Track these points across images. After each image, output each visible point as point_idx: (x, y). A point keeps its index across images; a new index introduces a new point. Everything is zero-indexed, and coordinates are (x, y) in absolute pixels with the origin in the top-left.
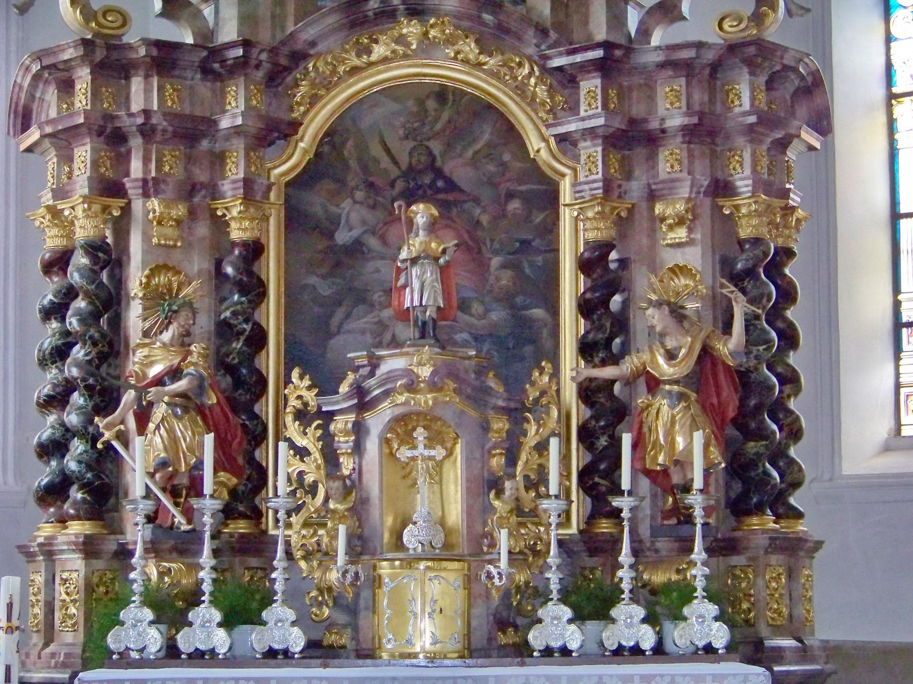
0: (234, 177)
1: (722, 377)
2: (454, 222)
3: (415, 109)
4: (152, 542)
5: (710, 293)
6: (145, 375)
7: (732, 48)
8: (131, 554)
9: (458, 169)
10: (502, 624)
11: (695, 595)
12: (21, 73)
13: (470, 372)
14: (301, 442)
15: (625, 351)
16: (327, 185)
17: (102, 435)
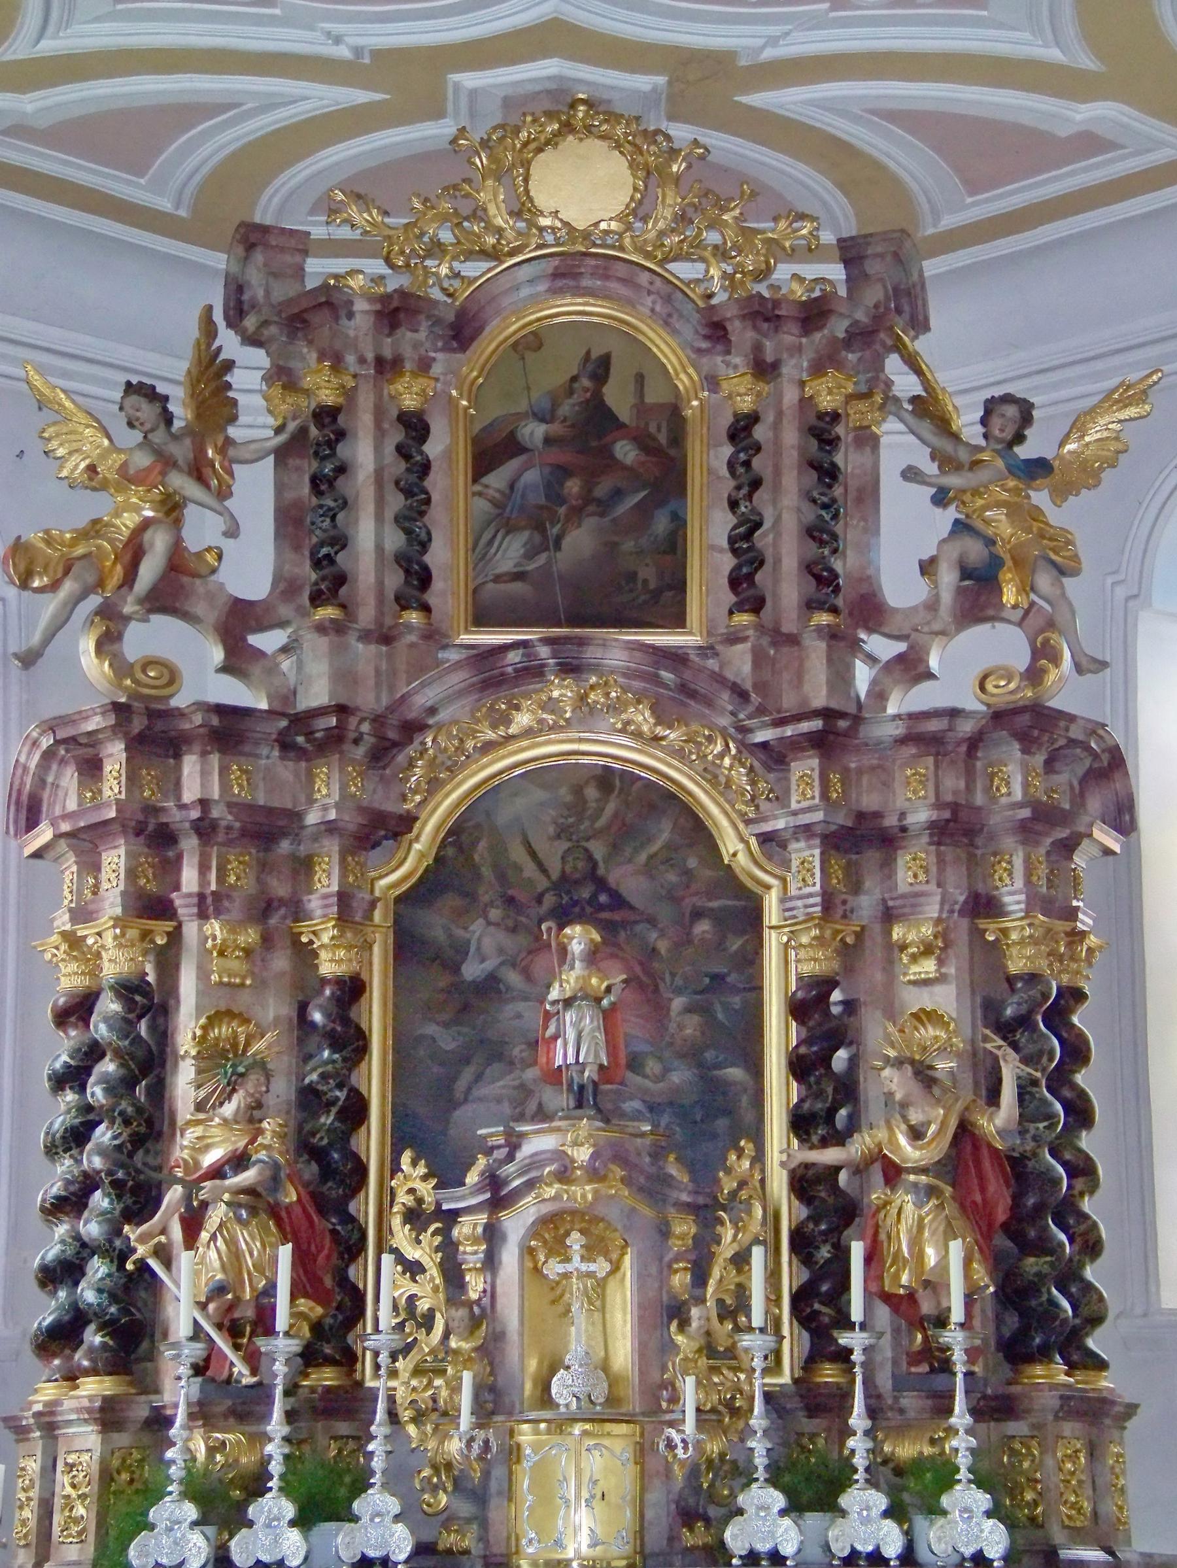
0: (325, 890)
1: (987, 1164)
2: (621, 949)
3: (569, 798)
4: (200, 1403)
5: (969, 1048)
6: (197, 1164)
7: (1000, 717)
8: (169, 1422)
9: (628, 879)
10: (688, 1516)
11: (957, 1477)
12: (26, 749)
13: (644, 1154)
14: (412, 1253)
15: (853, 1126)
16: (451, 901)
17: (134, 1250)
